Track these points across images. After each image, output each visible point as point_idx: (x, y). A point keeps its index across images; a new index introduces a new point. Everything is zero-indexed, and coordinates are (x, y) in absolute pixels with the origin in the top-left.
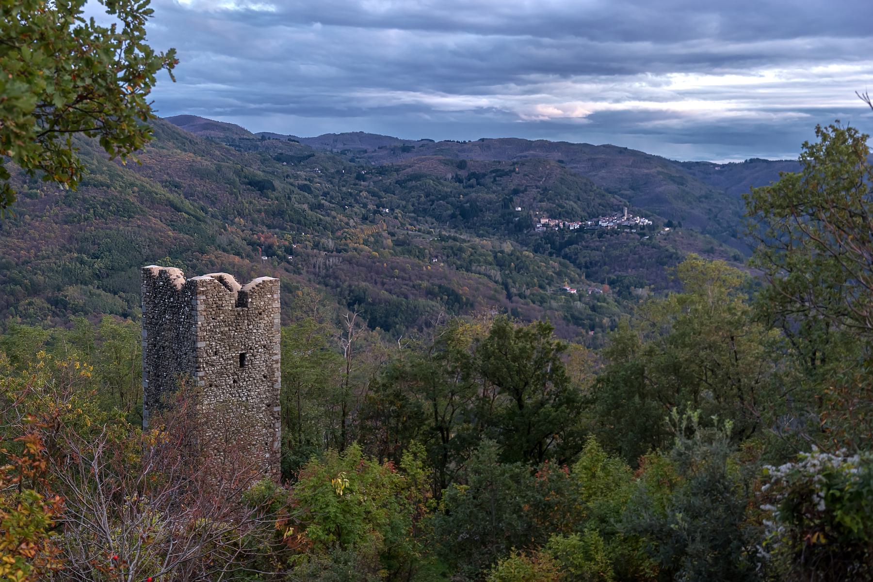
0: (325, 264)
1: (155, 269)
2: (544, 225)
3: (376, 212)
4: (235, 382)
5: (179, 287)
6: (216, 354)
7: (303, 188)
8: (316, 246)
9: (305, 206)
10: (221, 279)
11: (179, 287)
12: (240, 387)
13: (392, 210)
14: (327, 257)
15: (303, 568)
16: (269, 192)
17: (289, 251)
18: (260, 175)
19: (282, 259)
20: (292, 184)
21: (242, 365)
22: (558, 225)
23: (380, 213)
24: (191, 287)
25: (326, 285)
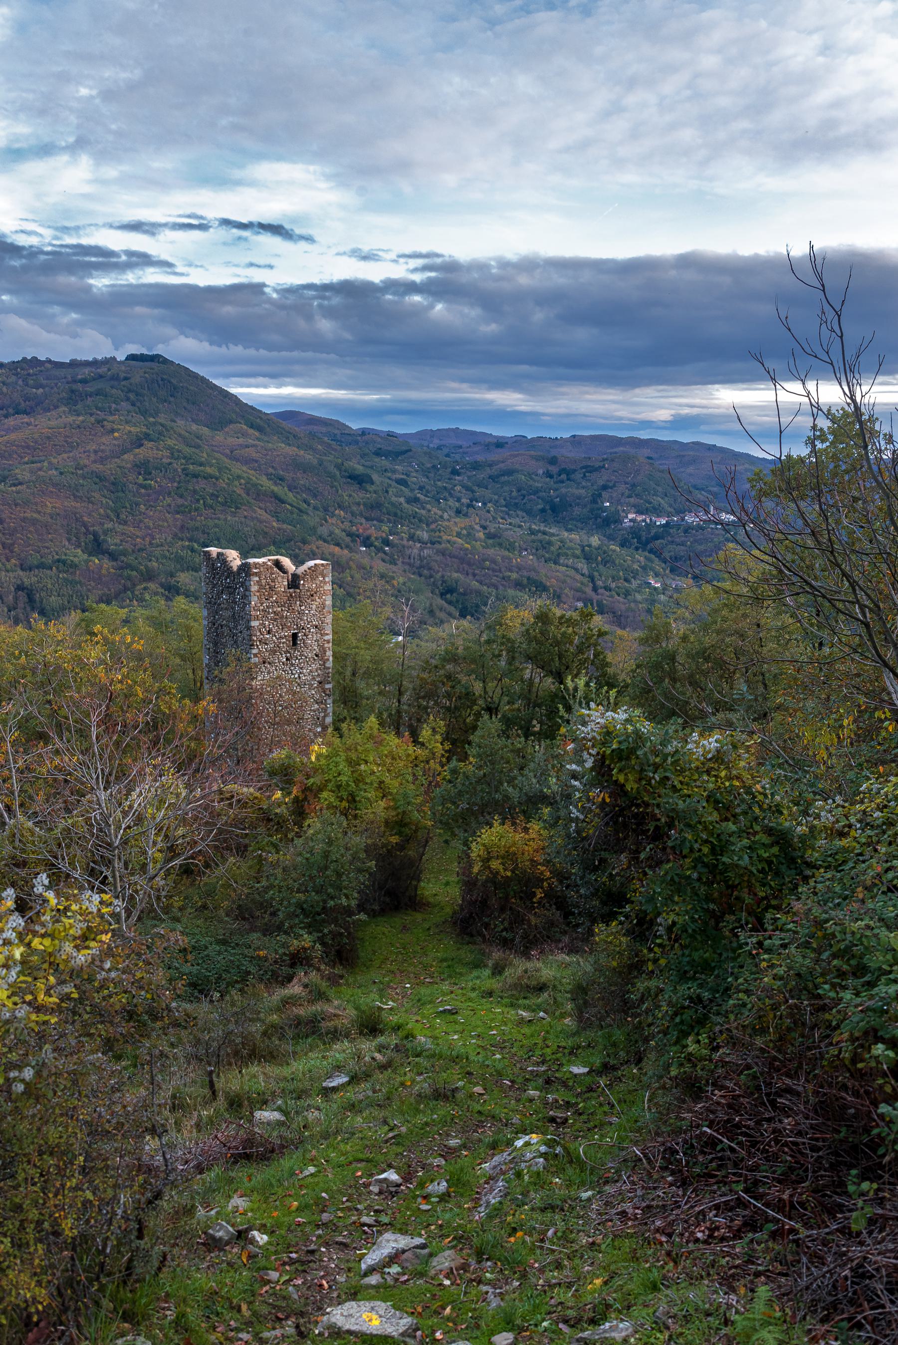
5: (235, 569)
6: (269, 632)
8: (412, 537)
9: (402, 500)
10: (277, 564)
11: (235, 569)
13: (484, 504)
14: (421, 549)
16: (368, 486)
17: (387, 542)
19: (379, 550)
22: (644, 521)
25: (420, 576)
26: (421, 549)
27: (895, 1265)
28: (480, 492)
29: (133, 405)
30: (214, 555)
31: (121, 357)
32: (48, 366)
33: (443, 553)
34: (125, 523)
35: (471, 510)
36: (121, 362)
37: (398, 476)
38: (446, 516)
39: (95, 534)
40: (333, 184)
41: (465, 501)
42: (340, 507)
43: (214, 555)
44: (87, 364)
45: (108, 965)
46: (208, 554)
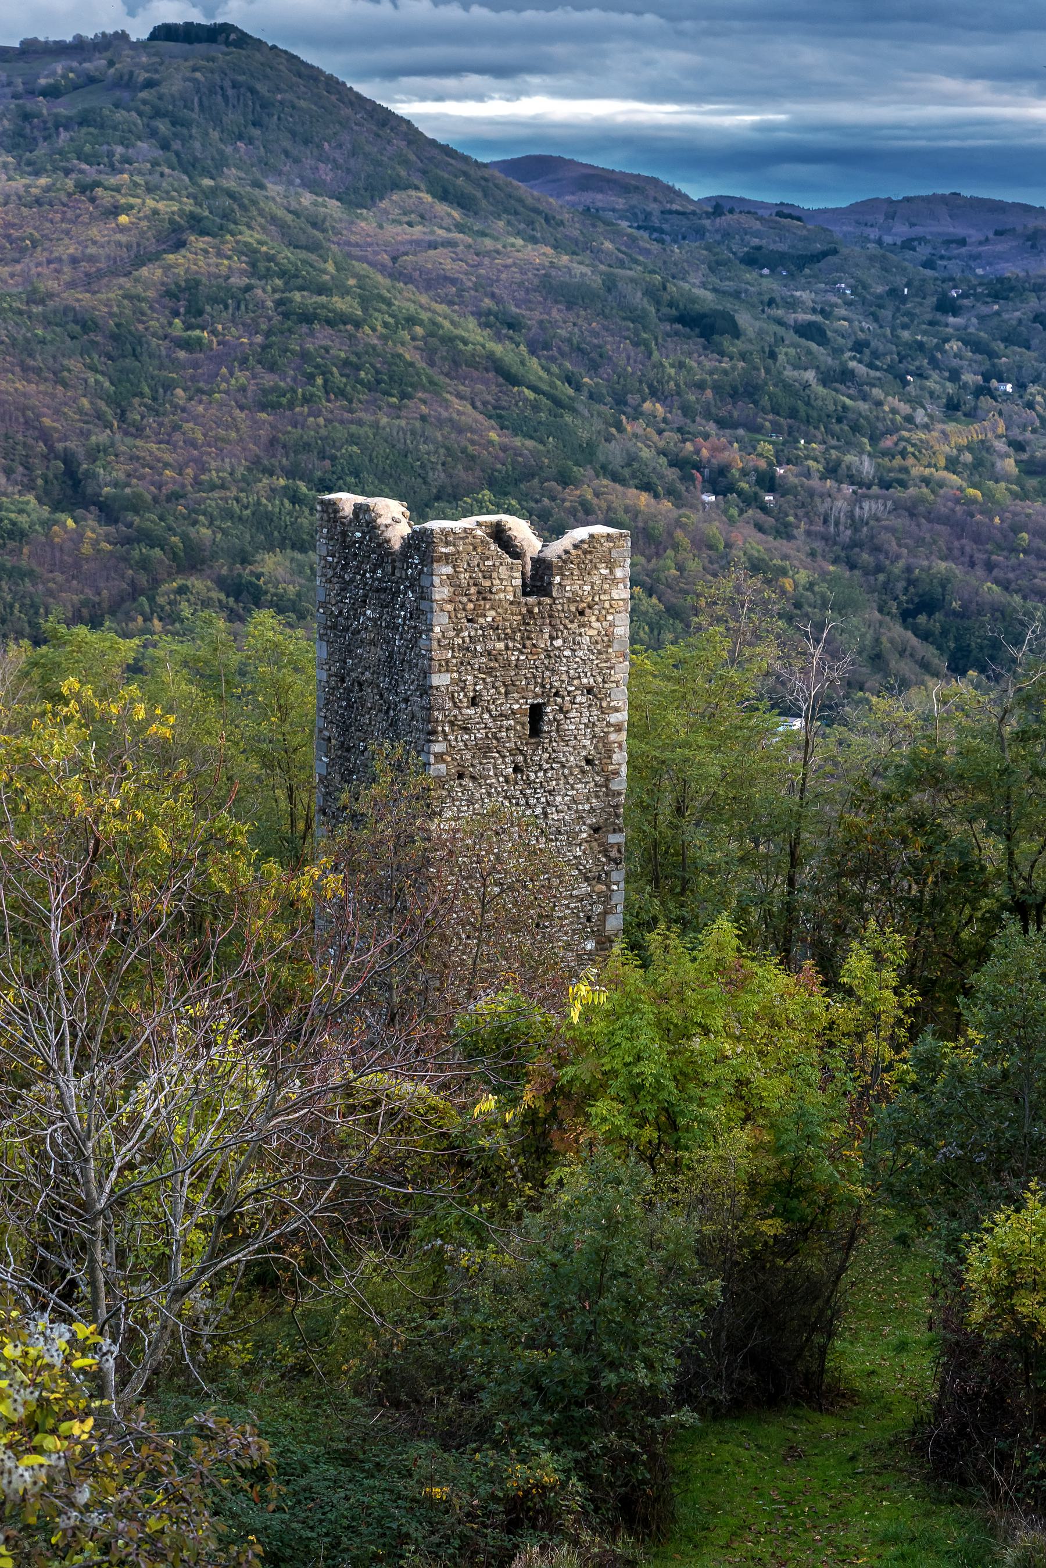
4: (517, 769)
5: (396, 545)
6: (474, 702)
7: (806, 331)
8: (832, 471)
10: (499, 535)
11: (396, 545)
12: (529, 783)
13: (1020, 386)
14: (857, 499)
17: (768, 482)
19: (751, 501)
20: (780, 322)
21: (535, 731)
23: (991, 393)
24: (420, 544)
26: (857, 499)
30: (348, 510)
36: (139, 45)
43: (348, 510)
44: (60, 50)
46: (332, 508)
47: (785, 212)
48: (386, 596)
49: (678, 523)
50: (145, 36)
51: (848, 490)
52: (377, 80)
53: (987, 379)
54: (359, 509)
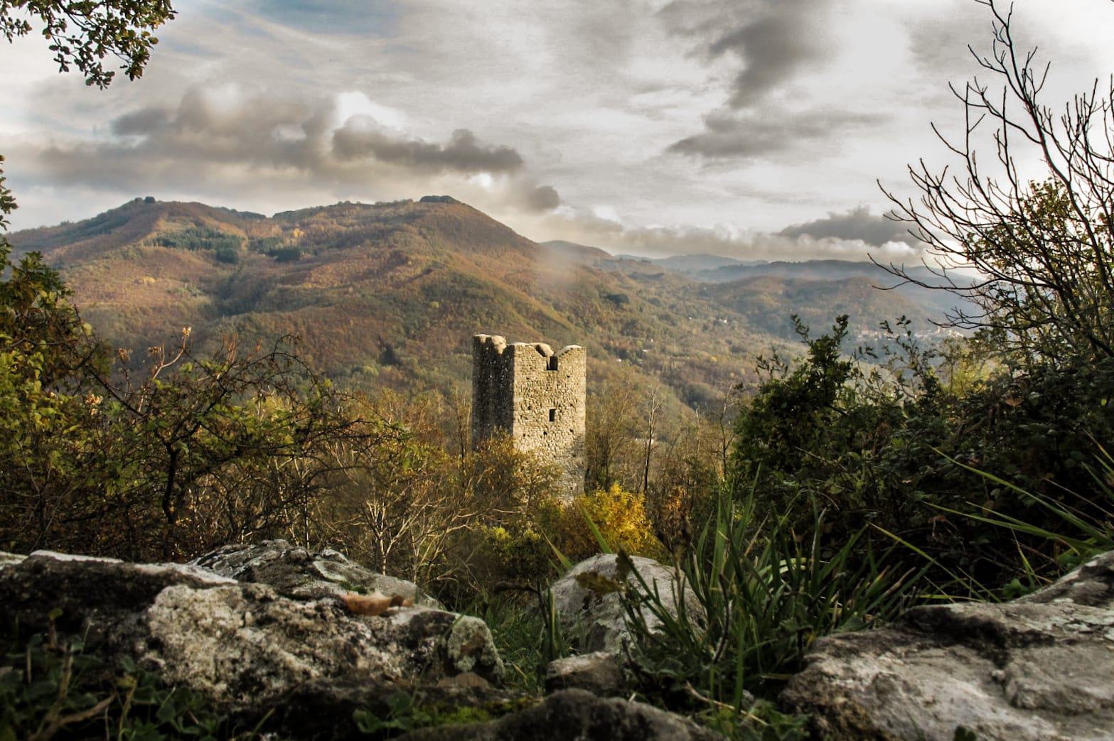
0: (670, 368)
1: (484, 337)
2: (865, 336)
3: (715, 323)
4: (545, 433)
5: (501, 352)
6: (529, 408)
7: (653, 301)
8: (663, 350)
9: (655, 317)
10: (538, 349)
11: (501, 352)
12: (549, 438)
13: (729, 321)
14: (672, 360)
15: (4, 355)
16: (625, 306)
17: (640, 355)
18: (616, 292)
19: (635, 362)
20: (644, 298)
21: (552, 419)
22: (876, 336)
23: (720, 324)
24: (510, 350)
25: (670, 385)
26: (672, 360)
27: (3, 550)
28: (725, 310)
29: (425, 238)
30: (484, 340)
31: (417, 199)
32: (358, 208)
33: (692, 365)
34: (414, 337)
35: (716, 328)
36: (417, 203)
37: (651, 297)
38: (694, 331)
39: (389, 347)
40: (651, 726)
41: (712, 319)
42: (600, 323)
43: (484, 340)
44: (389, 205)
45: (26, 596)
46: (478, 339)
47: (645, 262)
48: (497, 371)
49: (608, 369)
50: (419, 200)
51: (668, 357)
52: (492, 150)
53: (717, 318)
54: (489, 340)
